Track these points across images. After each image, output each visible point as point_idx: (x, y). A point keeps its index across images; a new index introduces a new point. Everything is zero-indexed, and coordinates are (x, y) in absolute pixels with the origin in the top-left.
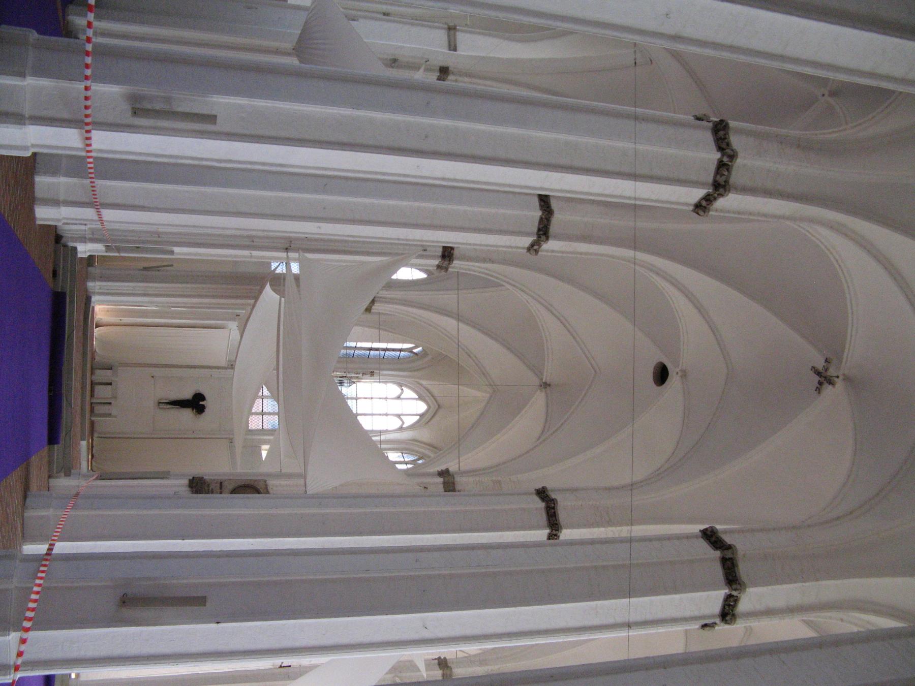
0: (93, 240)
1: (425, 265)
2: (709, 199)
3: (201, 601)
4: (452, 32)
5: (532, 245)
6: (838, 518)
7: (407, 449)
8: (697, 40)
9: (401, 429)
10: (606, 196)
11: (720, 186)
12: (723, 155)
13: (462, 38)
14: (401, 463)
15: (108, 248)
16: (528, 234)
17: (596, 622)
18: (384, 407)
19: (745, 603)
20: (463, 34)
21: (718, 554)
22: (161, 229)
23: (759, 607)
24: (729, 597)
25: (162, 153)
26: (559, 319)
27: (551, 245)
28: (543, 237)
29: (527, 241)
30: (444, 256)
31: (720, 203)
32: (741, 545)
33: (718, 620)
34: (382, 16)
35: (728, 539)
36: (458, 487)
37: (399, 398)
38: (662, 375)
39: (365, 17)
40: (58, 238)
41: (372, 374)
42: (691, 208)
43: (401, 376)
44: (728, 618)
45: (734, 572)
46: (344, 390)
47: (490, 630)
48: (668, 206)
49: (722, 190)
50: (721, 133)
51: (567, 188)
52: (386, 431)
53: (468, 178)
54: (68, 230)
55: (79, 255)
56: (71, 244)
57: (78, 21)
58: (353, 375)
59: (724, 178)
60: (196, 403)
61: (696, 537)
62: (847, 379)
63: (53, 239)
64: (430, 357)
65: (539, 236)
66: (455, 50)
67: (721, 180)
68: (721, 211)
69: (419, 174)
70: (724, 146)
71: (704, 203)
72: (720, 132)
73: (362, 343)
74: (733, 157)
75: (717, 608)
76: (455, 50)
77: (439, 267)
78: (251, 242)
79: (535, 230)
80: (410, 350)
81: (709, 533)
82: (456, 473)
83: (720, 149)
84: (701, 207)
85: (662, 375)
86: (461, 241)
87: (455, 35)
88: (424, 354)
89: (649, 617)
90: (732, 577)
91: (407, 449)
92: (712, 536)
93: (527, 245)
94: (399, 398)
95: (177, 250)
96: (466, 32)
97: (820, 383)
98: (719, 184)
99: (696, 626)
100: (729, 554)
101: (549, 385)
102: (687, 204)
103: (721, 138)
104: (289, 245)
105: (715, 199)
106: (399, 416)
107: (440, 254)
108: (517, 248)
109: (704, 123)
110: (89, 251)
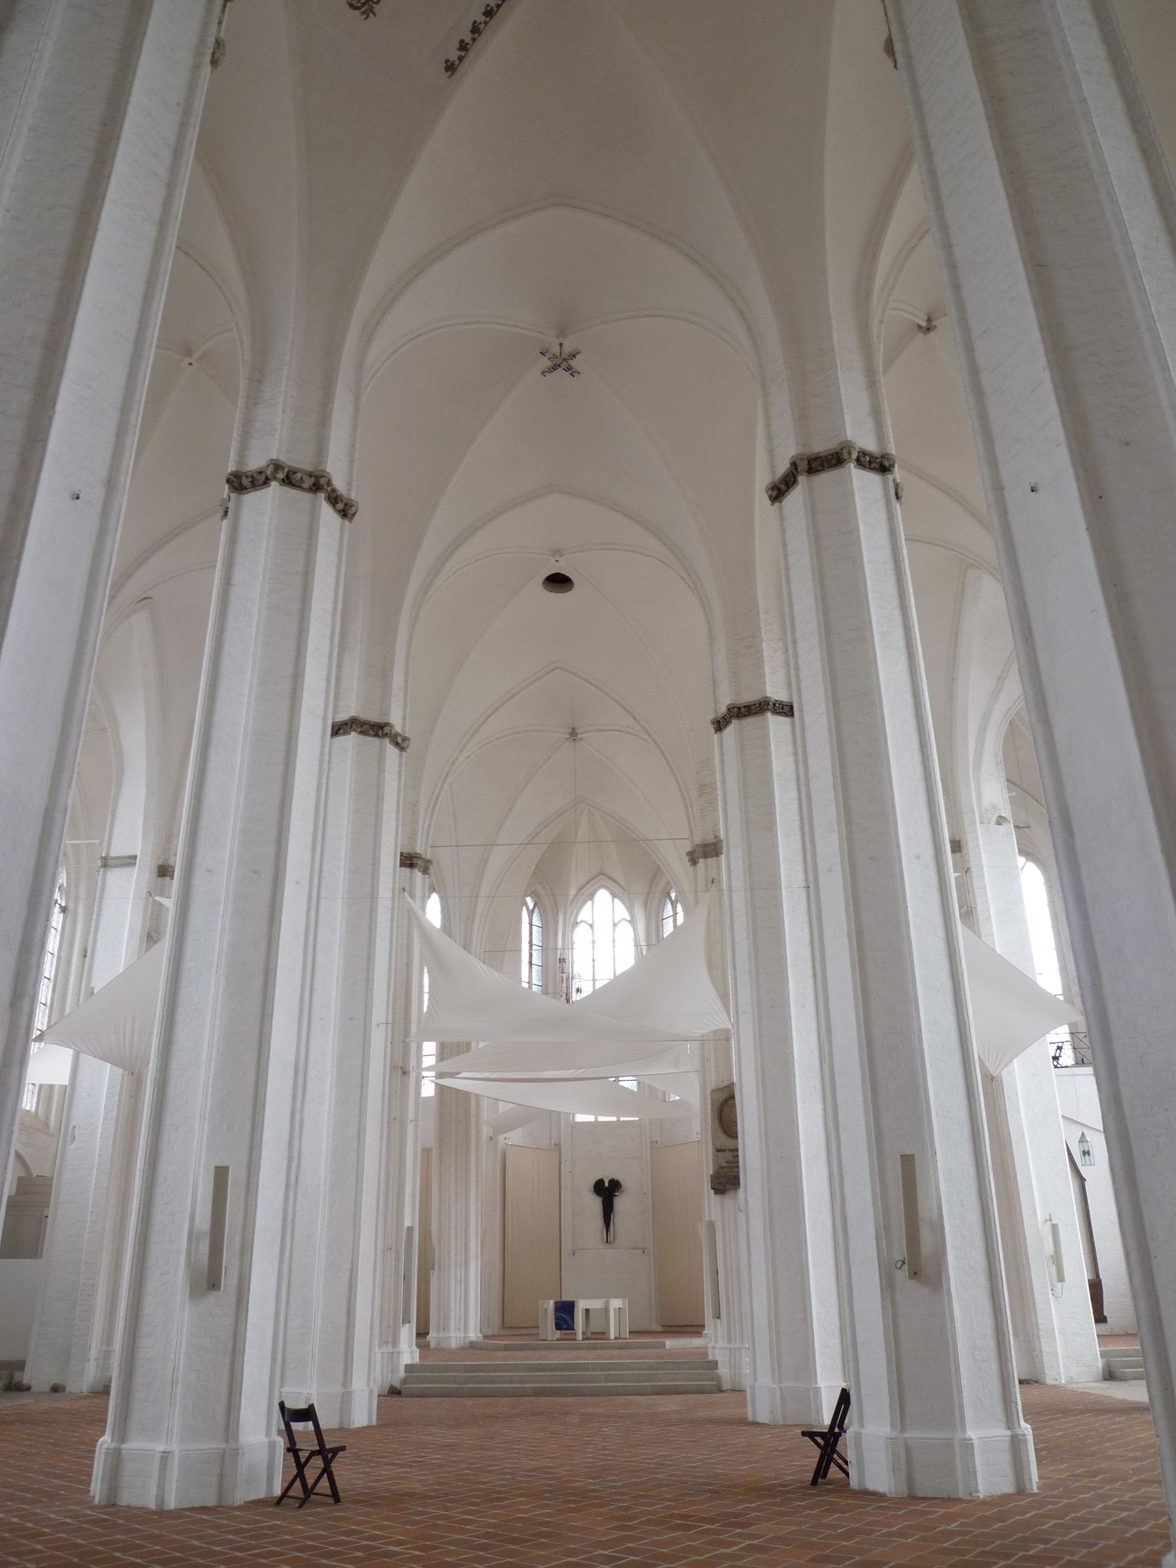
0: (395, 1343)
1: (423, 889)
2: (334, 499)
3: (908, 1162)
4: (110, 862)
5: (397, 744)
6: (749, 329)
7: (657, 916)
8: (114, 457)
9: (632, 922)
10: (333, 633)
11: (317, 483)
12: (275, 478)
13: (118, 849)
14: (675, 921)
15: (406, 1320)
16: (382, 750)
17: (899, 633)
18: (604, 940)
19: (870, 444)
20: (113, 847)
21: (802, 479)
22: (380, 1247)
23: (870, 425)
24: (860, 463)
25: (279, 1243)
26: (490, 716)
27: (396, 720)
28: (386, 730)
29: (391, 751)
30: (411, 866)
31: (339, 484)
32: (787, 452)
33: (890, 477)
34: (87, 959)
35: (783, 468)
36: (711, 839)
37: (591, 926)
38: (559, 581)
39: (89, 980)
40: (394, 1392)
41: (562, 961)
42: (347, 522)
43: (564, 924)
44: (887, 464)
45: (826, 457)
46: (587, 990)
47: (919, 769)
48: (342, 576)
49: (323, 481)
50: (245, 482)
51: (323, 685)
52: (636, 939)
53: (312, 816)
54: (381, 1378)
55: (417, 1360)
56: (402, 1373)
57: (84, 1379)
58: (564, 984)
59: (306, 478)
60: (607, 1191)
61: (781, 509)
62: (562, 333)
63: (396, 1399)
64: (539, 887)
65: (385, 735)
66: (135, 857)
67: (308, 482)
68: (350, 484)
69: (306, 884)
70: (262, 478)
71: (340, 506)
72: (241, 483)
73: (529, 975)
74: (277, 466)
75: (874, 478)
76: (135, 857)
77: (425, 871)
78: (395, 1121)
79: (376, 740)
80: (531, 913)
81: (775, 493)
82: (692, 842)
83: (266, 482)
84: (345, 510)
85: (559, 581)
86: (392, 847)
87: (114, 858)
88: (536, 896)
89: (890, 564)
90: (834, 460)
91: (657, 916)
92: (779, 489)
93: (396, 751)
94: (591, 926)
95: (407, 1223)
96: (109, 844)
97: (569, 369)
98: (315, 484)
99: (897, 506)
100: (803, 466)
101: (573, 729)
102: (342, 529)
103: (252, 482)
104: (402, 1070)
105: (334, 491)
106: (615, 925)
107: (408, 870)
108: (400, 764)
109: (231, 505)
110: (410, 1347)
